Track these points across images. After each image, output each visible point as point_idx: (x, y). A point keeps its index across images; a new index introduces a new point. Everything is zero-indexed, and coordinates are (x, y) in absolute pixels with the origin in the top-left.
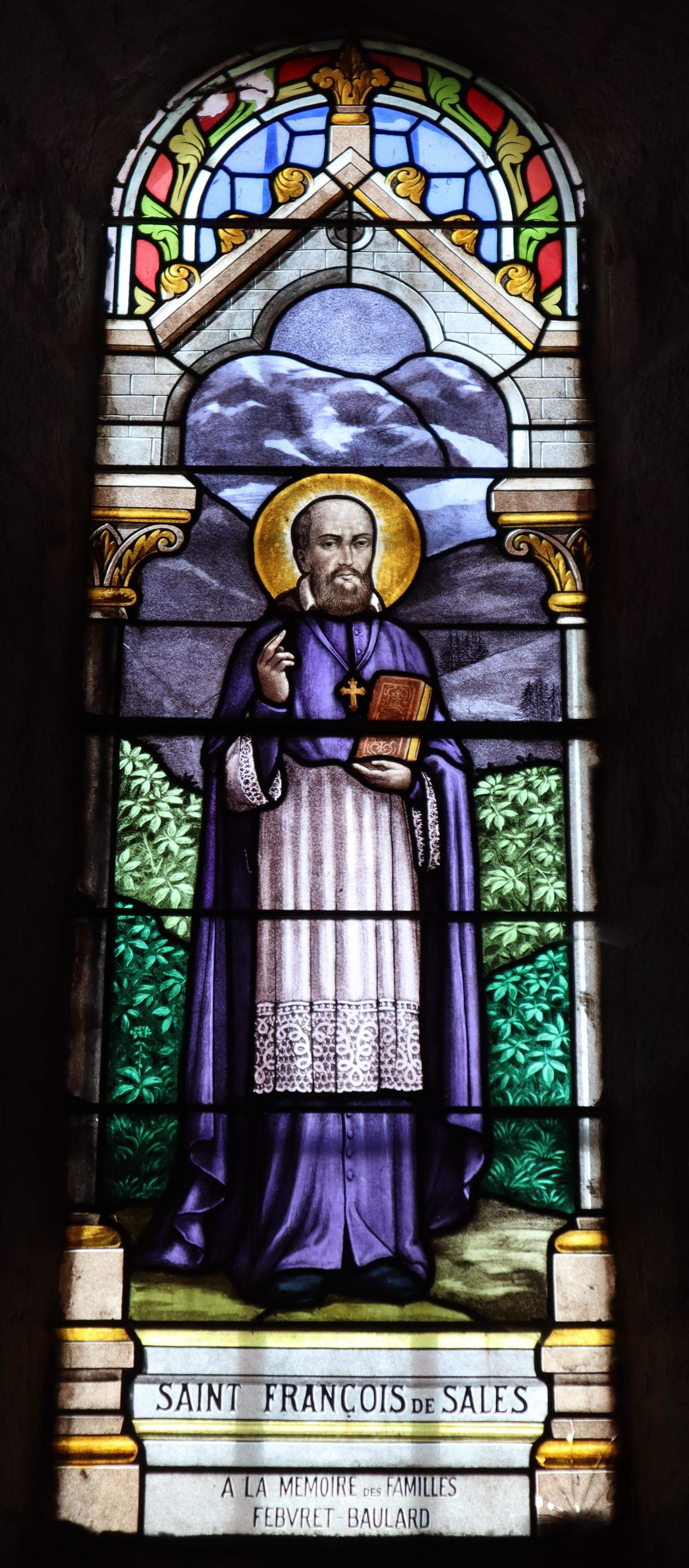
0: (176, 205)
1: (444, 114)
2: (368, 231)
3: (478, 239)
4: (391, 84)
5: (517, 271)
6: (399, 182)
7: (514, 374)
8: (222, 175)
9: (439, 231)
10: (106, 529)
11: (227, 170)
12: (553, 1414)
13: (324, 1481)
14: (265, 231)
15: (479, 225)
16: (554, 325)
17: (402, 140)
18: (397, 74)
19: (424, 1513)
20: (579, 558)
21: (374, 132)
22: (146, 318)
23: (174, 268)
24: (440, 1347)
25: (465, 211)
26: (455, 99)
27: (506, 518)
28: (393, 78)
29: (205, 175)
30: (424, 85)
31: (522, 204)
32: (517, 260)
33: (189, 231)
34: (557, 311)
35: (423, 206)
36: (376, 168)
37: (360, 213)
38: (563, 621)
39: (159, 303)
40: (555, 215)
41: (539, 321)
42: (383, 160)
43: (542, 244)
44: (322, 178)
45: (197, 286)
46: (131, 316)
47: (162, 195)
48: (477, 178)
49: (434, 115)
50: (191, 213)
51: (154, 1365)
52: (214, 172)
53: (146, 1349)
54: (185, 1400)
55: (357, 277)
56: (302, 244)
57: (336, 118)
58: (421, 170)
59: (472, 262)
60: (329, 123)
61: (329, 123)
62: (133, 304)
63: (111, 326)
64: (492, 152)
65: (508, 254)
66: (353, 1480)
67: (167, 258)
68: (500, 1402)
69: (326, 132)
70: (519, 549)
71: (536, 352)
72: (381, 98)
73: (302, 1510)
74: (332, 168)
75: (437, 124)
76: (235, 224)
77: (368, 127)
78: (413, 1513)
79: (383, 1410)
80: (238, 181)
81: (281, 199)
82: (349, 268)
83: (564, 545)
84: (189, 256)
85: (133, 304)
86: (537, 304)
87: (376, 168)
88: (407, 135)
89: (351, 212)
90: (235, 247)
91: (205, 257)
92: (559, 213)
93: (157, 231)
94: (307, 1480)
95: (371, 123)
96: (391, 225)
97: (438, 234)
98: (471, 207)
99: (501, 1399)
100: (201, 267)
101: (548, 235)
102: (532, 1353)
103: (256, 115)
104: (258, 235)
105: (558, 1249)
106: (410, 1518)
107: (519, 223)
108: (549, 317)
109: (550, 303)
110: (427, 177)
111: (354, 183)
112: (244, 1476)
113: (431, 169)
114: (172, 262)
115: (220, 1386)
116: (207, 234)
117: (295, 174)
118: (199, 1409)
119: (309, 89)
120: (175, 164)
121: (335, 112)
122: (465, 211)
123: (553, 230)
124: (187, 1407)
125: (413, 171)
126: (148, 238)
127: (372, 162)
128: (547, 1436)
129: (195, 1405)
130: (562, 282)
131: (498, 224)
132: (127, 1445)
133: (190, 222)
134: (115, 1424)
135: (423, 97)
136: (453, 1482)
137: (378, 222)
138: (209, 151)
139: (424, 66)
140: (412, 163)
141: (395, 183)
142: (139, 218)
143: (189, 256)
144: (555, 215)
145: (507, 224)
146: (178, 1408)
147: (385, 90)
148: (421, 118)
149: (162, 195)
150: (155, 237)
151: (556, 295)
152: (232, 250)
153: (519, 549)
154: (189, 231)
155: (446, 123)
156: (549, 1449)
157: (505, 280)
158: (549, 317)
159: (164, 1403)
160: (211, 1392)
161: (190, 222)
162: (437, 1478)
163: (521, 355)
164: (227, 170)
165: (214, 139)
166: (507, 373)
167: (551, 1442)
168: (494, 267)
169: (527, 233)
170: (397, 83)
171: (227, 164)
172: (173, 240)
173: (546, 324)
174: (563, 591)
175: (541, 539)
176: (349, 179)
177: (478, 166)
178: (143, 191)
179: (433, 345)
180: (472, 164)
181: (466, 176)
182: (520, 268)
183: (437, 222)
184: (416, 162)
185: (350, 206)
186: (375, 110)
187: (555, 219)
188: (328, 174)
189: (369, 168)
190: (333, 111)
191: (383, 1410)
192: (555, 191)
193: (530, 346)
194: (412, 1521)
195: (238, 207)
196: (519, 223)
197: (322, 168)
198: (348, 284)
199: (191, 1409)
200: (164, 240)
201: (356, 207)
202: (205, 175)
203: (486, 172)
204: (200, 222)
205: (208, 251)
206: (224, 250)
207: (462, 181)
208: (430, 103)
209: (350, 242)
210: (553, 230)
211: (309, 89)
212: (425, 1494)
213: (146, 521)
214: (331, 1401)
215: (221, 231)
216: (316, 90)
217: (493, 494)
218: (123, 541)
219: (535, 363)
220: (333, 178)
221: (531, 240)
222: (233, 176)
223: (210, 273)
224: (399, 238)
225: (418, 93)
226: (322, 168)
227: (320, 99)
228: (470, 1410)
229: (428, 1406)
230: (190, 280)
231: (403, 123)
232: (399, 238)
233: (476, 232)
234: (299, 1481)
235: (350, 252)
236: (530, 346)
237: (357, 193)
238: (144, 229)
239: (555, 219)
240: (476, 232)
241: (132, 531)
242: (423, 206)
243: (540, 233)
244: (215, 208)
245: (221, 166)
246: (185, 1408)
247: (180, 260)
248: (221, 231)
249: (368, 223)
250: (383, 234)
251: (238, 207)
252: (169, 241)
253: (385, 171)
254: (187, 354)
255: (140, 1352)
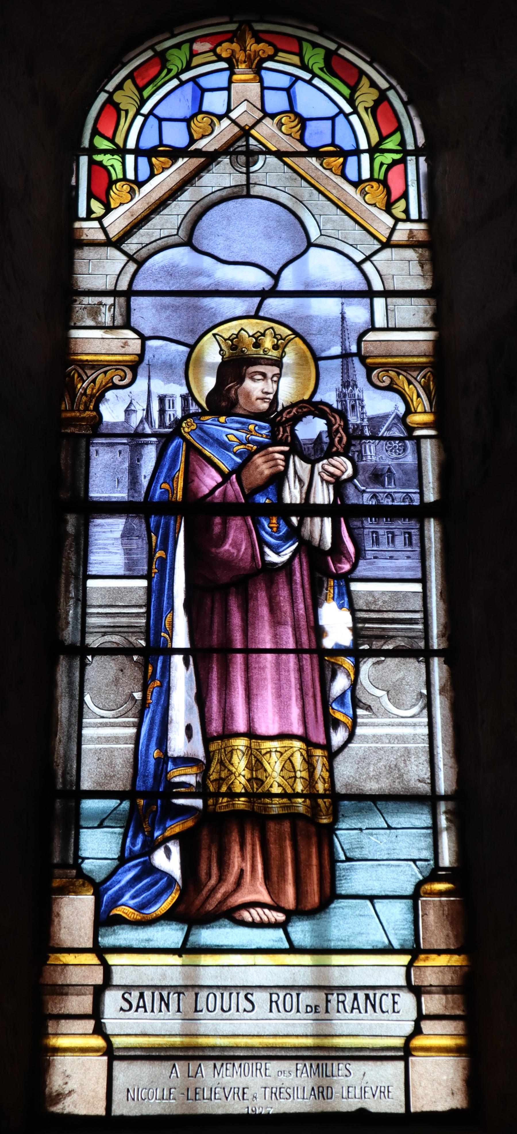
0: (119, 140)
1: (314, 75)
2: (261, 158)
3: (344, 164)
4: (275, 54)
5: (372, 187)
6: (283, 124)
7: (372, 259)
8: (152, 120)
9: (314, 159)
10: (74, 369)
11: (156, 117)
12: (421, 1017)
13: (247, 1065)
14: (186, 159)
15: (344, 154)
16: (400, 226)
17: (284, 94)
18: (279, 46)
19: (329, 1089)
20: (426, 388)
21: (263, 88)
22: (100, 219)
23: (119, 184)
24: (333, 964)
25: (333, 144)
26: (322, 65)
27: (369, 361)
28: (277, 50)
29: (140, 120)
30: (300, 54)
31: (375, 138)
32: (372, 179)
33: (130, 159)
34: (403, 216)
35: (302, 140)
36: (266, 115)
37: (256, 146)
38: (418, 433)
39: (108, 209)
40: (399, 145)
41: (390, 222)
42: (270, 108)
43: (390, 167)
44: (226, 122)
45: (137, 198)
46: (88, 218)
47: (110, 134)
48: (341, 120)
49: (307, 76)
50: (131, 144)
51: (116, 980)
52: (146, 117)
53: (113, 968)
54: (141, 1004)
55: (255, 190)
56: (161, 211)
57: (235, 77)
58: (298, 115)
59: (340, 181)
60: (230, 81)
61: (230, 81)
62: (90, 211)
63: (77, 225)
64: (351, 102)
65: (366, 174)
66: (267, 1065)
67: (114, 177)
68: (396, 1005)
69: (228, 89)
70: (384, 382)
71: (387, 244)
72: (269, 64)
73: (388, 1087)
74: (233, 115)
75: (309, 82)
76: (164, 154)
77: (259, 84)
78: (321, 1089)
79: (298, 1011)
80: (165, 124)
81: (196, 137)
82: (248, 184)
83: (416, 379)
84: (131, 175)
85: (90, 211)
86: (388, 209)
87: (266, 115)
88: (288, 90)
89: (248, 145)
90: (164, 169)
91: (142, 178)
92: (403, 143)
93: (106, 159)
94: (234, 1065)
95: (261, 81)
96: (280, 155)
97: (313, 160)
98: (337, 142)
99: (397, 1003)
100: (141, 184)
101: (394, 160)
102: (404, 969)
103: (177, 76)
104: (181, 162)
105: (422, 894)
106: (319, 1092)
107: (373, 151)
108: (397, 220)
109: (398, 209)
110: (303, 121)
111: (250, 125)
112: (186, 1063)
113: (306, 114)
114: (118, 180)
115: (169, 994)
116: (143, 161)
117: (125, 187)
118: (153, 1011)
119: (214, 58)
120: (118, 111)
121: (234, 73)
122: (333, 144)
123: (397, 156)
124: (143, 1009)
125: (292, 116)
126: (100, 164)
127: (263, 110)
128: (417, 1031)
129: (149, 1008)
130: (405, 195)
131: (357, 152)
132: (98, 1042)
133: (130, 152)
134: (89, 1025)
135: (298, 63)
136: (348, 1066)
137: (268, 152)
138: (143, 102)
139: (300, 40)
140: (292, 110)
141: (280, 125)
142: (92, 150)
143: (131, 175)
144: (399, 145)
145: (364, 151)
146: (136, 1011)
147: (271, 58)
148: (298, 78)
149: (110, 134)
150: (105, 163)
151: (402, 204)
152: (163, 172)
153: (384, 382)
154: (130, 159)
155: (316, 81)
156: (418, 1042)
157: (364, 193)
158: (397, 220)
159: (126, 1006)
160: (162, 998)
161: (130, 152)
162: (335, 1063)
163: (378, 246)
164: (156, 117)
165: (146, 93)
166: (368, 258)
167: (422, 1036)
168: (355, 185)
169: (379, 158)
170: (280, 54)
171: (156, 112)
172: (118, 166)
173: (395, 225)
174: (416, 412)
175: (399, 374)
176: (246, 121)
177: (341, 111)
178: (95, 132)
179: (313, 239)
180: (337, 110)
181: (332, 119)
182: (375, 184)
183: (314, 152)
184: (296, 110)
185: (247, 141)
186: (264, 73)
187: (399, 148)
188: (230, 118)
189: (261, 115)
190: (232, 73)
191: (298, 1011)
192: (400, 129)
193: (384, 240)
194: (320, 1094)
195: (165, 142)
196: (373, 151)
197: (226, 115)
198: (249, 196)
199: (146, 1011)
200: (112, 166)
201: (252, 141)
202: (140, 120)
203: (347, 116)
204: (138, 152)
205: (144, 172)
206: (156, 172)
207: (329, 122)
208: (304, 67)
209: (248, 165)
210: (397, 156)
211: (214, 58)
212: (326, 1076)
213: (106, 363)
214: (374, 1006)
215: (154, 160)
216: (220, 59)
217: (363, 344)
218: (88, 377)
219: (386, 253)
220: (233, 121)
221: (382, 164)
222: (161, 120)
223: (146, 189)
224: (285, 163)
225: (296, 59)
226: (226, 115)
227: (223, 65)
228: (357, 1011)
229: (316, 1009)
230: (132, 192)
231: (284, 81)
232: (285, 163)
233: (341, 160)
234: (228, 1065)
235: (248, 173)
236: (384, 240)
237: (253, 132)
238: (98, 158)
239: (399, 148)
240: (341, 160)
241: (93, 371)
242: (302, 140)
243: (388, 158)
244: (149, 141)
245: (151, 113)
246: (141, 1010)
247: (125, 179)
248: (154, 160)
249: (262, 153)
250: (272, 160)
251: (165, 142)
252: (115, 166)
253: (273, 116)
254: (132, 246)
255: (108, 970)
